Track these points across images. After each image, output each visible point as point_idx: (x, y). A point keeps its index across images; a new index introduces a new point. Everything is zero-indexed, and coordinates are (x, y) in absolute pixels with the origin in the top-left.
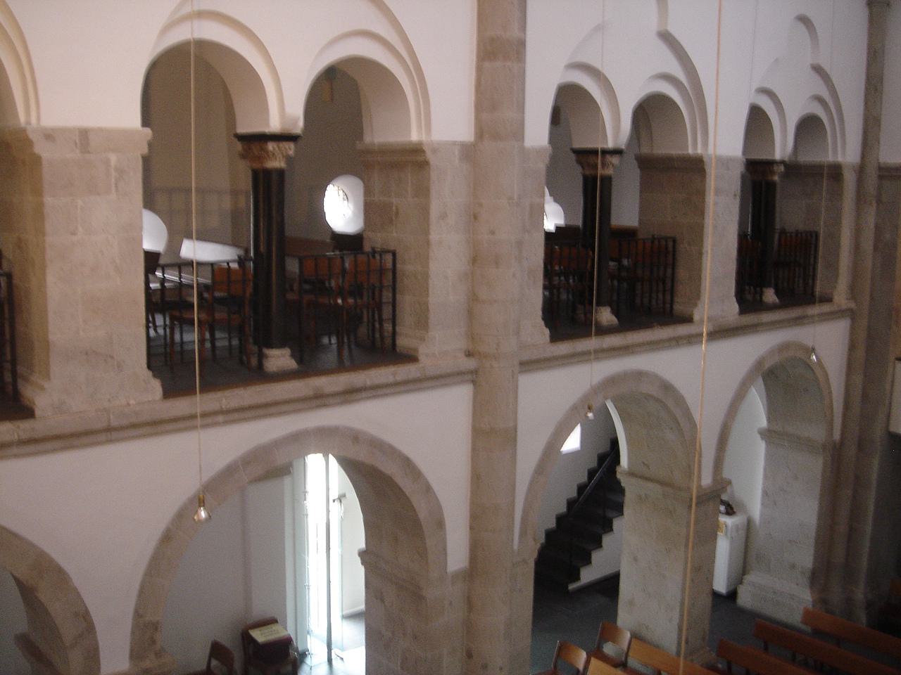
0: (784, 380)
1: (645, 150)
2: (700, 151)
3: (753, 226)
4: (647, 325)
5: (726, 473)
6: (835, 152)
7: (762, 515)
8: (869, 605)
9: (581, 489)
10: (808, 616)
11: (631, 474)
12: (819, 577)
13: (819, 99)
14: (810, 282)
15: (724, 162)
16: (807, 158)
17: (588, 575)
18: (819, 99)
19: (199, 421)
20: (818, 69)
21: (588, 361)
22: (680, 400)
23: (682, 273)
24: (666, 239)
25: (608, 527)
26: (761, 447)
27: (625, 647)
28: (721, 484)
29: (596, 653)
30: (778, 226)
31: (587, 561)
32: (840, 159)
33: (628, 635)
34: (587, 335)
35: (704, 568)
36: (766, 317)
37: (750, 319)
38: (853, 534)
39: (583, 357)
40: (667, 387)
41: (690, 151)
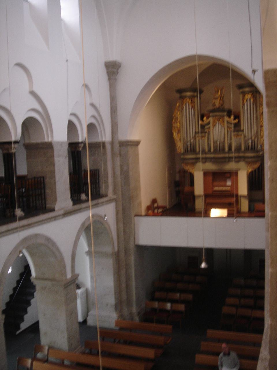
0: (93, 231)
1: (27, 141)
2: (50, 140)
3: (73, 170)
4: (36, 214)
5: (77, 271)
6: (102, 137)
7: (92, 286)
8: (139, 314)
9: (15, 289)
10: (117, 323)
11: (37, 278)
12: (118, 306)
13: (93, 117)
14: (98, 189)
15: (61, 144)
16: (94, 140)
17: (24, 326)
18: (93, 117)
19: (18, 229)
20: (92, 105)
21: (17, 232)
22: (54, 244)
23: (48, 191)
24: (40, 177)
25: (29, 304)
26: (87, 259)
27: (46, 353)
28: (75, 277)
29: (34, 359)
30: (83, 169)
31: (22, 320)
32: (104, 140)
33: (47, 348)
34: (16, 221)
35: (73, 313)
36: (84, 205)
37: (77, 207)
38: (128, 286)
39: (15, 230)
40: (48, 239)
41: (46, 140)
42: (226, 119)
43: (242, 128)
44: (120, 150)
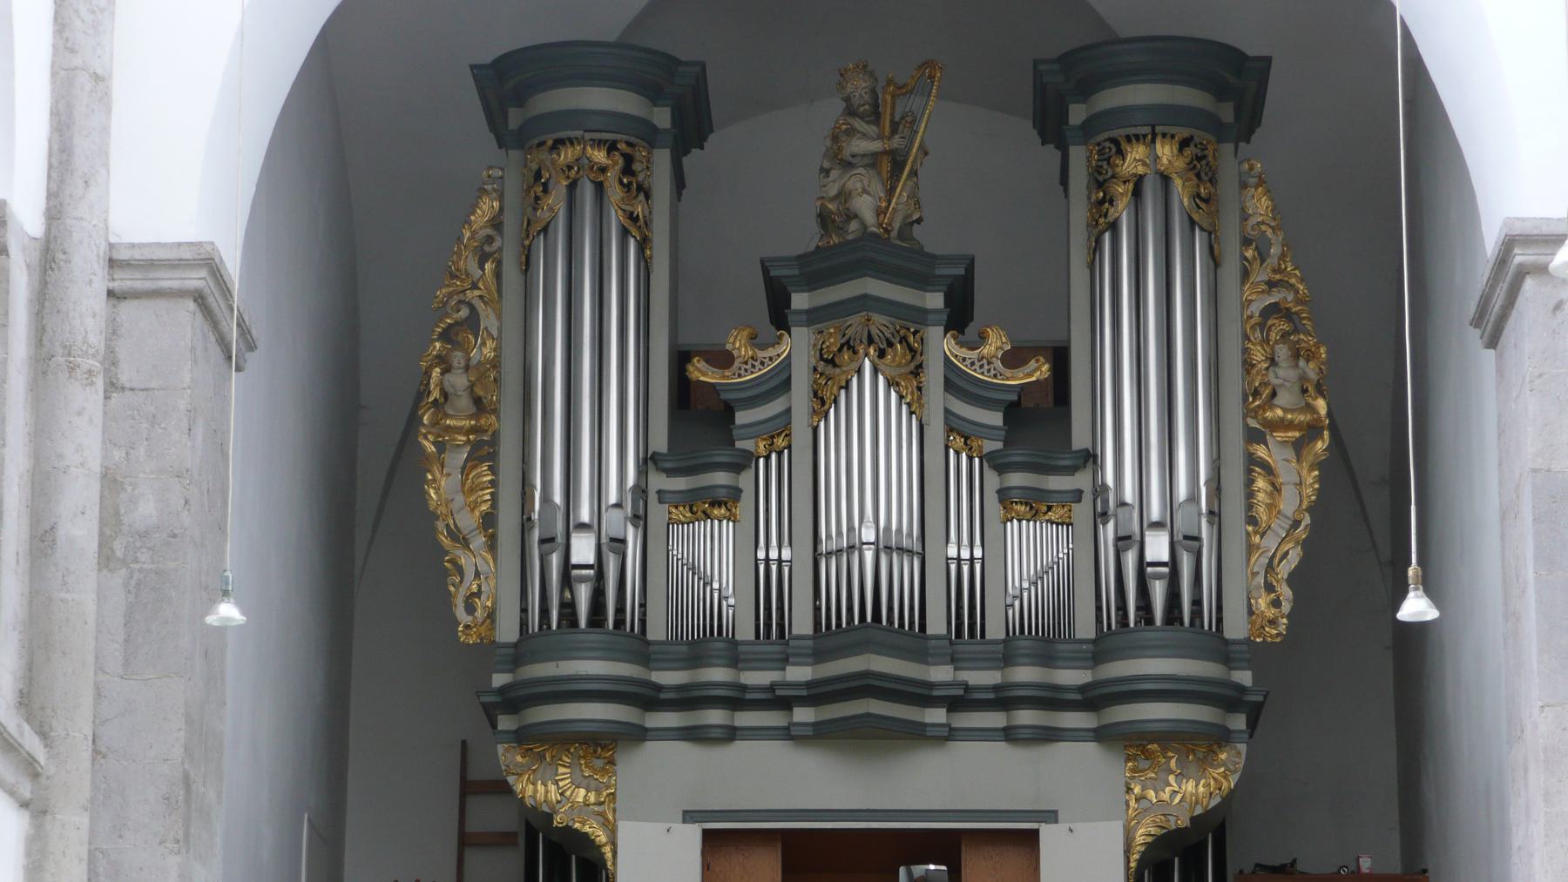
42: (942, 345)
43: (1080, 440)
44: (113, 331)
